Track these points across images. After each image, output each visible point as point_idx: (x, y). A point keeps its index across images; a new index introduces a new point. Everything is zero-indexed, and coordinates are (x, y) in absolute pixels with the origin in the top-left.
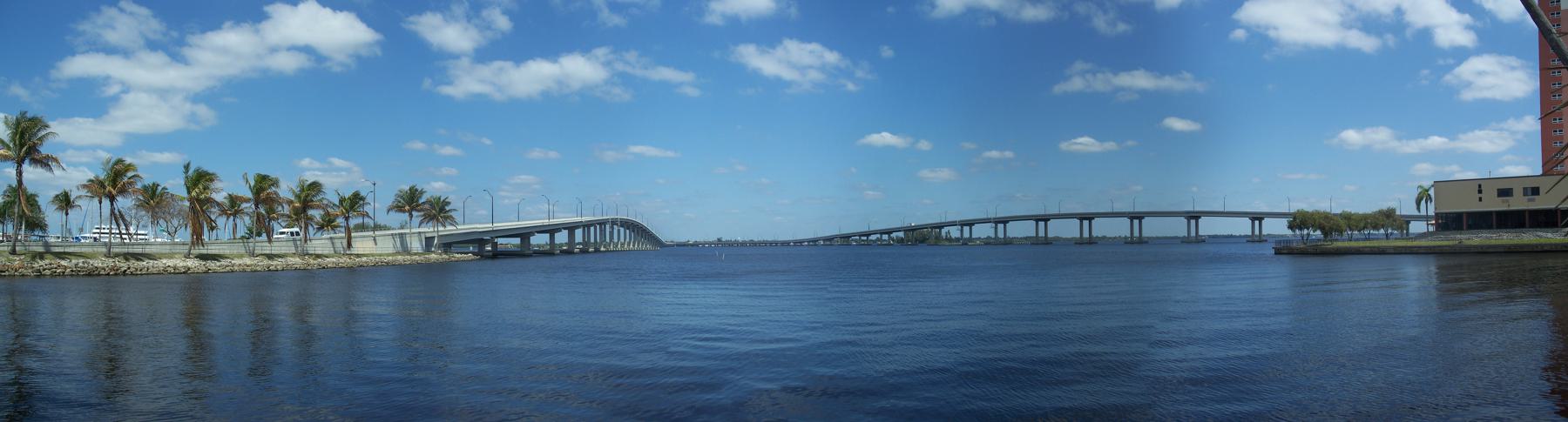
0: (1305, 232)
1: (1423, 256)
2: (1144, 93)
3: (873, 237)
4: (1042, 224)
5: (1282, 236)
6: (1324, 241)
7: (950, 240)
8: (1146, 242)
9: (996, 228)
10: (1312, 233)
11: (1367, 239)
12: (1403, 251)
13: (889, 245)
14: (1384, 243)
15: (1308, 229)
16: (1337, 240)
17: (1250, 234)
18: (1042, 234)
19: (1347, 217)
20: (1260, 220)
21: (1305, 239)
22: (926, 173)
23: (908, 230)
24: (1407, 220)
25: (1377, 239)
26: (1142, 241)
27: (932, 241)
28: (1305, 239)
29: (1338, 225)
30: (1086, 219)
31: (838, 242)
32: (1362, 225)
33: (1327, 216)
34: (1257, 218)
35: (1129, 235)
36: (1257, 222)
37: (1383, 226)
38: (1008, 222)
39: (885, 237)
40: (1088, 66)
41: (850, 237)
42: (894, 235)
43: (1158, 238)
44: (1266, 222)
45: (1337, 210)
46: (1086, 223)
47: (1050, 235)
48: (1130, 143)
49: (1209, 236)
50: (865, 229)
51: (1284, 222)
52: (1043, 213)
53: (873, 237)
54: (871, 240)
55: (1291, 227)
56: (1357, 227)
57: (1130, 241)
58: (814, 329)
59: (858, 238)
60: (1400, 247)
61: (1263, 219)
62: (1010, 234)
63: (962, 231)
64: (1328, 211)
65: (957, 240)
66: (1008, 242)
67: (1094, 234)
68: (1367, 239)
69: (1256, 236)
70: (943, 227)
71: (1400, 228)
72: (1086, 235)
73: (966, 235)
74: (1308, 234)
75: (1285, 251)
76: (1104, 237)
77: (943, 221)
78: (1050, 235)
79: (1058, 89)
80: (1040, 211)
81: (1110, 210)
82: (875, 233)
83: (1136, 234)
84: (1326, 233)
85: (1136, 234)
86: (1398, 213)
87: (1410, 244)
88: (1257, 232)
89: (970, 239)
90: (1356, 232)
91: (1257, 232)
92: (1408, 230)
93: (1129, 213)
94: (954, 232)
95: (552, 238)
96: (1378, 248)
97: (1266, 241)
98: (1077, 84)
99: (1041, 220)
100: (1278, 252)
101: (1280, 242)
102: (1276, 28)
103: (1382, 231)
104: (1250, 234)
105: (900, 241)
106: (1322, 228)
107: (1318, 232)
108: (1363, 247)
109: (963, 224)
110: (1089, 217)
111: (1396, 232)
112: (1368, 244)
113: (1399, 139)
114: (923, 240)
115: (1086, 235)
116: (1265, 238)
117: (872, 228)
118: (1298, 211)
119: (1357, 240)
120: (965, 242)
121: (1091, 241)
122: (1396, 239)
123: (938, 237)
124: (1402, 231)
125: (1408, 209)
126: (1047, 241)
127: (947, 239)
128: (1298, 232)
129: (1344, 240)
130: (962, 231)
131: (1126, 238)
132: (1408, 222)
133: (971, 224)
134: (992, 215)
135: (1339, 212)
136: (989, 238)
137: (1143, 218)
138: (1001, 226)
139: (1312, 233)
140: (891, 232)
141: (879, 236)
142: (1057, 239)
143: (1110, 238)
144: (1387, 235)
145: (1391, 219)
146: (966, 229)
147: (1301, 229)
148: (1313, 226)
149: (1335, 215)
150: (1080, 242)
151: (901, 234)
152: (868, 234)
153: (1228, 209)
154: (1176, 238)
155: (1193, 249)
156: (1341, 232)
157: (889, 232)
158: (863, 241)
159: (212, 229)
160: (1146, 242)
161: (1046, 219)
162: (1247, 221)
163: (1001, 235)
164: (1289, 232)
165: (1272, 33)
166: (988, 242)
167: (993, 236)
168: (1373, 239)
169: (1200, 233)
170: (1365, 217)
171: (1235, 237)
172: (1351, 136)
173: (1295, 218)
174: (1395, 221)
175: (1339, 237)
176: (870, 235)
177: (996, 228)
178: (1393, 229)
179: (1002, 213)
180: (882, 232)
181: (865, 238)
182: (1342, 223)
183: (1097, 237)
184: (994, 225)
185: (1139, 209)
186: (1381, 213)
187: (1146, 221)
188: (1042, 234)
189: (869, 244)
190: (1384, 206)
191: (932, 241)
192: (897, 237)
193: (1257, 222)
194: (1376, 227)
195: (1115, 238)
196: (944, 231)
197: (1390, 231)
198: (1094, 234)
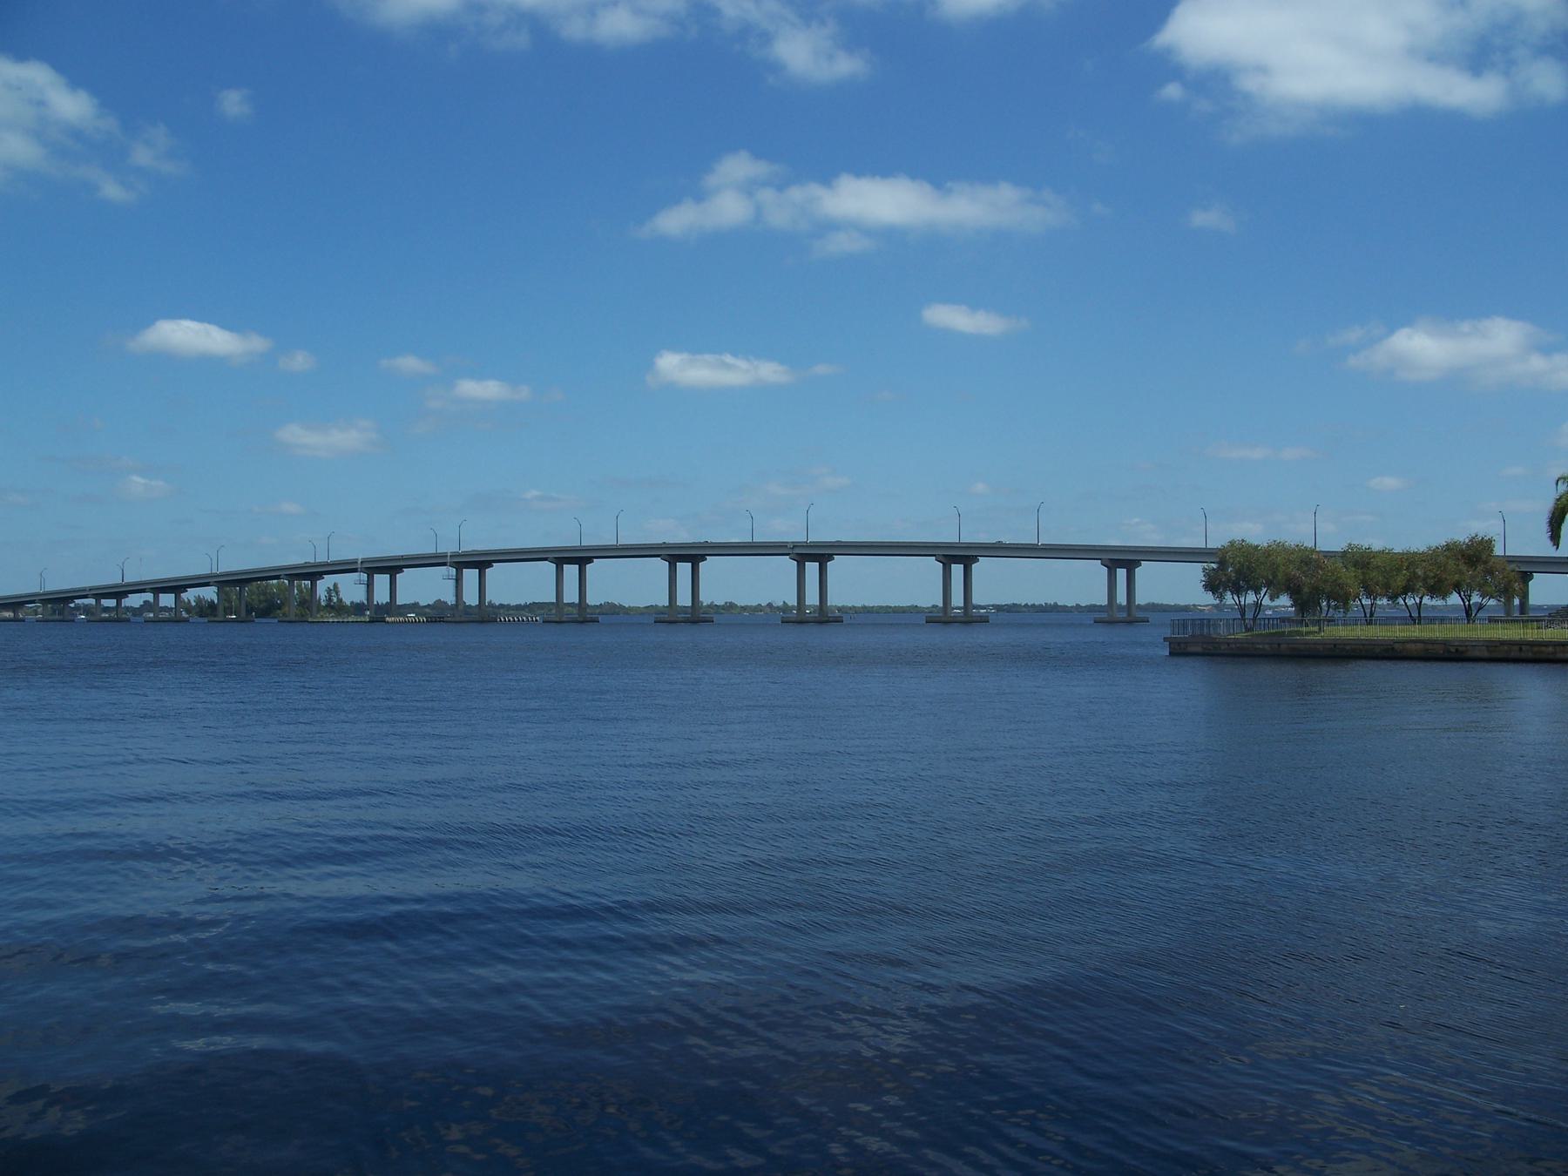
0: (1251, 598)
1: (1530, 666)
2: (890, 236)
3: (134, 601)
4: (571, 571)
5: (1186, 609)
6: (1301, 622)
7: (337, 608)
8: (838, 620)
9: (458, 580)
10: (1266, 601)
11: (1415, 618)
12: (1514, 654)
13: (179, 621)
14: (1460, 632)
15: (1257, 592)
16: (1331, 621)
17: (1105, 602)
18: (571, 595)
19: (1360, 560)
20: (1131, 566)
21: (1249, 615)
22: (294, 434)
23: (227, 582)
24: (1525, 569)
25: (1442, 620)
26: (825, 617)
27: (292, 610)
28: (1249, 615)
29: (1341, 586)
30: (683, 558)
31: (35, 612)
32: (1400, 581)
33: (1308, 559)
34: (1122, 561)
35: (793, 601)
36: (1121, 573)
37: (1457, 587)
38: (489, 564)
39: (167, 600)
40: (761, 169)
41: (72, 599)
42: (190, 595)
43: (866, 610)
44: (1144, 571)
45: (1332, 539)
46: (684, 569)
47: (592, 600)
48: (821, 369)
49: (999, 608)
50: (112, 579)
51: (1194, 573)
52: (573, 542)
53: (134, 601)
54: (127, 608)
55: (1212, 585)
56: (1387, 586)
57: (796, 618)
58: (458, 849)
59: (92, 601)
60: (1503, 643)
61: (1137, 563)
62: (495, 596)
63: (370, 586)
64: (1309, 544)
65: (358, 608)
66: (486, 615)
67: (706, 598)
68: (1415, 618)
69: (1120, 607)
70: (320, 575)
71: (1505, 592)
72: (684, 599)
73: (381, 596)
74: (1258, 606)
75: (1199, 649)
76: (730, 607)
77: (322, 558)
78: (592, 600)
79: (676, 221)
80: (565, 537)
81: (1029, 539)
82: (139, 588)
83: (812, 598)
84: (1305, 603)
85: (812, 598)
86: (1498, 551)
87: (1531, 634)
88: (1122, 599)
89: (391, 607)
90: (1385, 601)
91: (1122, 599)
92: (1524, 596)
93: (795, 545)
94: (351, 589)
95: (177, 598)
96: (1445, 643)
97: (595, 621)
98: (729, 209)
99: (571, 561)
100: (1179, 650)
101: (1184, 624)
102: (1262, 69)
103: (1454, 599)
104: (1105, 602)
105: (206, 610)
106: (1293, 590)
107: (1284, 601)
108: (1404, 642)
109: (373, 568)
110: (693, 555)
111: (1492, 602)
112: (1415, 632)
113: (1546, 350)
114: (268, 609)
115: (684, 599)
116: (1140, 615)
117: (131, 577)
118: (1232, 543)
119: (1388, 621)
120: (381, 614)
121: (697, 616)
122: (1491, 620)
123: (308, 602)
124: (1509, 600)
125: (1528, 540)
126: (585, 615)
127: (330, 607)
128: (1229, 599)
129: (1355, 622)
130: (370, 586)
131: (785, 608)
132: (1526, 577)
133: (393, 568)
134: (448, 547)
135: (1338, 545)
136: (439, 605)
137: (830, 557)
138: (470, 575)
139: (1266, 601)
140: (184, 588)
141: (149, 597)
142: (612, 610)
143: (744, 608)
144: (1468, 610)
145: (1480, 568)
146: (381, 581)
147: (1237, 591)
148: (1269, 584)
149: (1329, 555)
150: (668, 617)
151: (210, 594)
152: (119, 593)
153: (625, 540)
154: (914, 610)
155: (815, 637)
156: (1342, 598)
157: (177, 587)
158: (107, 609)
159: (1269, 555)
160: (838, 620)
161: (582, 558)
162: (1097, 570)
163: (471, 598)
164: (1209, 599)
165: (1249, 84)
166: (437, 615)
167: (450, 599)
168: (1432, 620)
169: (977, 599)
170: (1408, 561)
171: (1065, 609)
172: (670, 363)
173: (1222, 563)
174: (1490, 572)
175: (1339, 615)
176: (125, 594)
177: (458, 580)
178: (1483, 596)
179: (477, 541)
180: (159, 588)
181: (111, 603)
182: (1349, 577)
183: (711, 606)
184: (364, 576)
185: (823, 534)
186: (1451, 549)
187: (837, 566)
188: (571, 595)
189: (120, 618)
190: (1461, 533)
191: (292, 610)
192: (199, 600)
193: (1121, 573)
194: (1437, 589)
195: (759, 608)
196: (323, 586)
197: (1476, 598)
198: (706, 598)
